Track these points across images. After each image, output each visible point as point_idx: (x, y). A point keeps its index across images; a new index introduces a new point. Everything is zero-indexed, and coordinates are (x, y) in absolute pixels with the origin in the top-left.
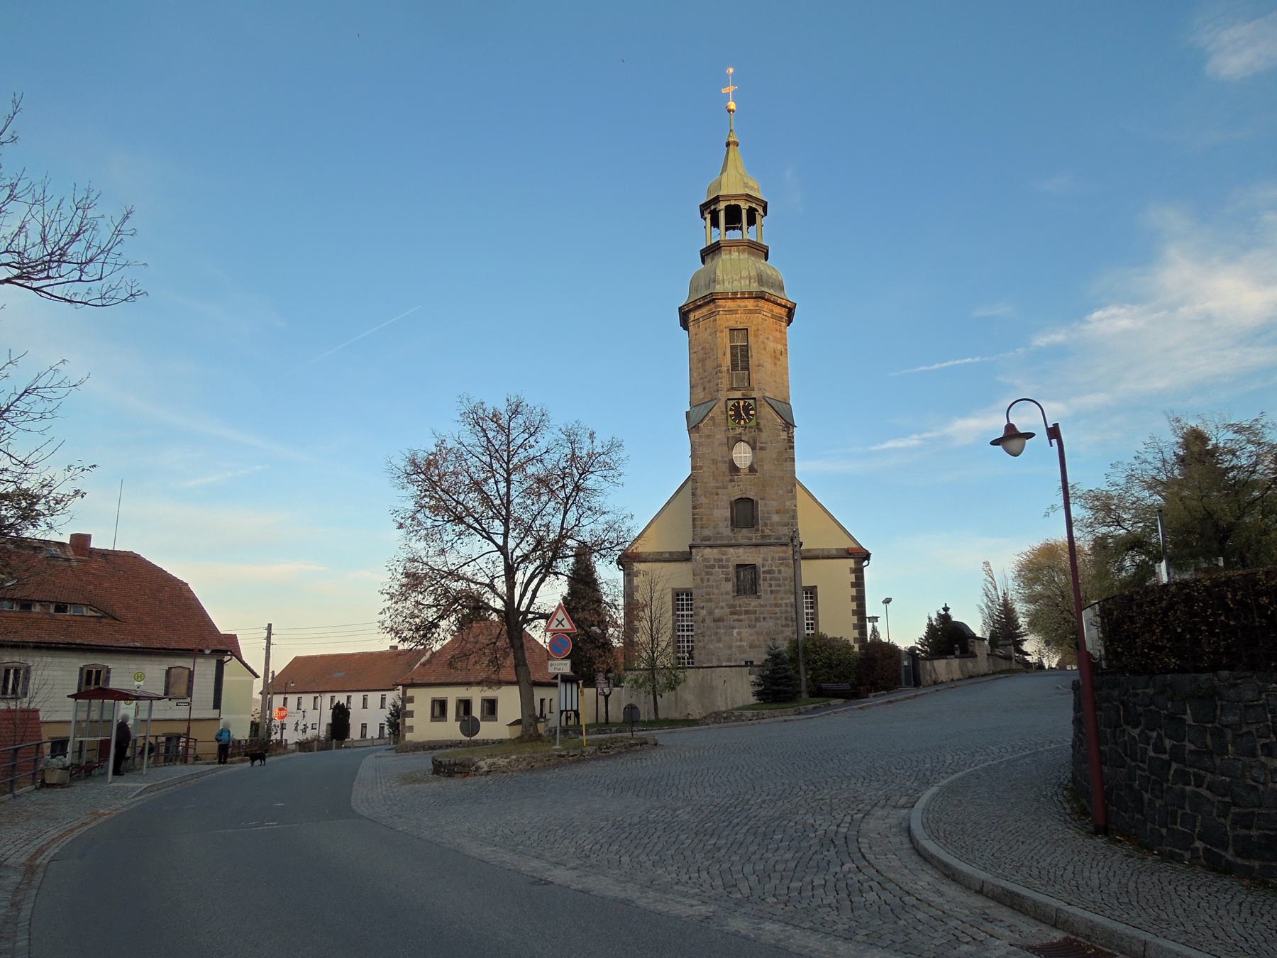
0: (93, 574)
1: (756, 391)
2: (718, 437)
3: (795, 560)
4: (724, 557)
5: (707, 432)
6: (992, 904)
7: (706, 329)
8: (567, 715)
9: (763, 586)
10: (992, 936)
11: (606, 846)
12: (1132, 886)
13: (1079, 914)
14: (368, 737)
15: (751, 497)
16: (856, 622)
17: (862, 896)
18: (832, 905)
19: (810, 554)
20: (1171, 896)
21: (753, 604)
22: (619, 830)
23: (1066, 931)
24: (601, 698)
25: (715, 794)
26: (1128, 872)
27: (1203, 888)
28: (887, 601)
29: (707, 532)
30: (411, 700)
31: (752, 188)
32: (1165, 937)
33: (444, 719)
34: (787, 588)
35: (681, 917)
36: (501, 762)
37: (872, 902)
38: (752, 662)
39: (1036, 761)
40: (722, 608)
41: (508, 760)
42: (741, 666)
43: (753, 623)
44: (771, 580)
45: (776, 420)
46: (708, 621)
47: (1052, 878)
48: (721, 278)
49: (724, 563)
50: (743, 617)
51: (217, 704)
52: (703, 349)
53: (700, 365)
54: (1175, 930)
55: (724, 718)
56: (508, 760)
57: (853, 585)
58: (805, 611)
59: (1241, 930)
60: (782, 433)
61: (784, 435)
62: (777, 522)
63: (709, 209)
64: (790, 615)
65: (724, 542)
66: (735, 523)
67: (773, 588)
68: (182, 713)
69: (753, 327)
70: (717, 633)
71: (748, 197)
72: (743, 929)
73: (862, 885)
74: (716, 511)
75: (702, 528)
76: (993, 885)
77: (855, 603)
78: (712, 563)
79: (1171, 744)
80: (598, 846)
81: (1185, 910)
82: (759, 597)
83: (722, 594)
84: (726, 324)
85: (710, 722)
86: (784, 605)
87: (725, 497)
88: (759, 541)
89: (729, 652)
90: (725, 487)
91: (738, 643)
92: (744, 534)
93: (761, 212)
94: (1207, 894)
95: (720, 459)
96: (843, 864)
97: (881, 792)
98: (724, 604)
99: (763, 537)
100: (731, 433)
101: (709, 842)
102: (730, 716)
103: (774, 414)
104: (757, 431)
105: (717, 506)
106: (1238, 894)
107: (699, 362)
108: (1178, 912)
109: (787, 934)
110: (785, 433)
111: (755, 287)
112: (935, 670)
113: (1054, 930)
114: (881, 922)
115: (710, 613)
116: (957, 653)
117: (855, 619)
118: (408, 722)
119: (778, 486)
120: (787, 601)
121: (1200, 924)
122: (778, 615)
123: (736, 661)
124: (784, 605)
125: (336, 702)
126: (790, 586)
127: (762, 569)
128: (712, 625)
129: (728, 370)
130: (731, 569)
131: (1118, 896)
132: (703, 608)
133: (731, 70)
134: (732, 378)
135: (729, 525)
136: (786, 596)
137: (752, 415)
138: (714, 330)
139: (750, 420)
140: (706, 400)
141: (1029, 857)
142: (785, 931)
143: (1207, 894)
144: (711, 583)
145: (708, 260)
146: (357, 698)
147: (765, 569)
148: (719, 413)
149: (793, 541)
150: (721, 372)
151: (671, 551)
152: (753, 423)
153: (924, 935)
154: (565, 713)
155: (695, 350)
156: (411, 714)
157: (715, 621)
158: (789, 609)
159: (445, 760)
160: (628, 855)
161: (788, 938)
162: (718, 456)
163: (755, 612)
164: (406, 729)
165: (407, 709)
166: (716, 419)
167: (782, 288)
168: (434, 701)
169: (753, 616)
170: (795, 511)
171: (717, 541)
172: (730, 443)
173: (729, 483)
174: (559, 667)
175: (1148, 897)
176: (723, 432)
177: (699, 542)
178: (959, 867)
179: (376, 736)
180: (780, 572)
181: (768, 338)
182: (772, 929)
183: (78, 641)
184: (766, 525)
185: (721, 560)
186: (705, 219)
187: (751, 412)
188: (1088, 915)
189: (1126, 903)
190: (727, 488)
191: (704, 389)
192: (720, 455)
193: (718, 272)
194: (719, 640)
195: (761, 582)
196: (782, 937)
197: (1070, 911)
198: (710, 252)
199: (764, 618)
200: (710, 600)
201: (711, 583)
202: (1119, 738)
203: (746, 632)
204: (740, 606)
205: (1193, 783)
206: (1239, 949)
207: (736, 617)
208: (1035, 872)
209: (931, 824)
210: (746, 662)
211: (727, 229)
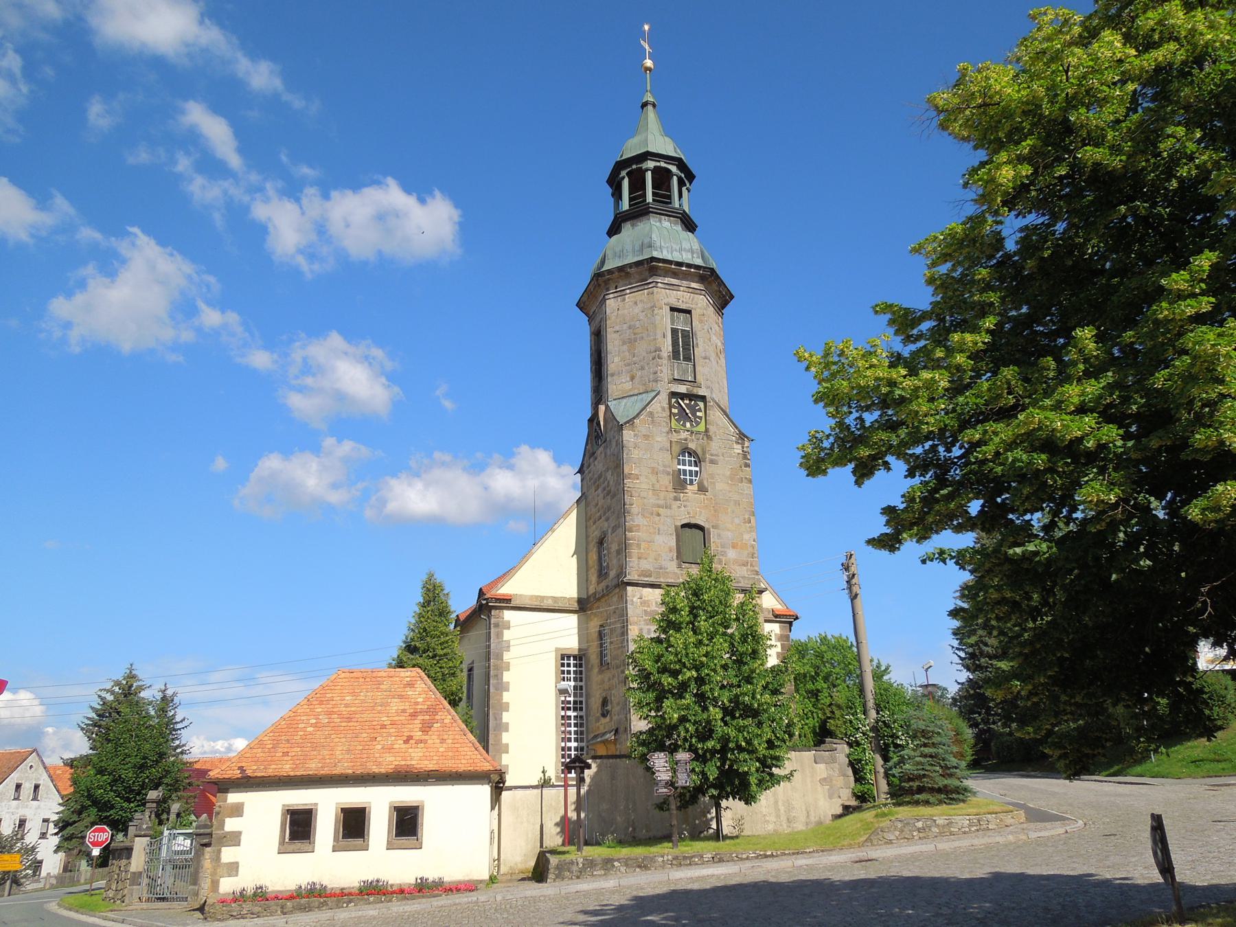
2: (659, 439)
5: (644, 431)
7: (636, 303)
15: (702, 524)
29: (646, 565)
33: (359, 841)
45: (728, 428)
48: (658, 244)
55: (919, 830)
60: (736, 446)
61: (738, 449)
69: (698, 310)
75: (639, 558)
84: (666, 301)
85: (892, 837)
90: (668, 507)
100: (675, 437)
103: (725, 421)
104: (705, 438)
105: (659, 530)
107: (624, 343)
110: (739, 446)
118: (228, 854)
133: (646, 27)
135: (675, 557)
138: (649, 305)
139: (698, 424)
140: (636, 392)
148: (660, 409)
150: (660, 357)
151: (555, 596)
152: (701, 428)
155: (617, 328)
166: (656, 415)
171: (659, 578)
172: (673, 448)
173: (674, 502)
176: (665, 434)
177: (636, 577)
190: (670, 508)
191: (632, 378)
192: (661, 463)
193: (654, 237)
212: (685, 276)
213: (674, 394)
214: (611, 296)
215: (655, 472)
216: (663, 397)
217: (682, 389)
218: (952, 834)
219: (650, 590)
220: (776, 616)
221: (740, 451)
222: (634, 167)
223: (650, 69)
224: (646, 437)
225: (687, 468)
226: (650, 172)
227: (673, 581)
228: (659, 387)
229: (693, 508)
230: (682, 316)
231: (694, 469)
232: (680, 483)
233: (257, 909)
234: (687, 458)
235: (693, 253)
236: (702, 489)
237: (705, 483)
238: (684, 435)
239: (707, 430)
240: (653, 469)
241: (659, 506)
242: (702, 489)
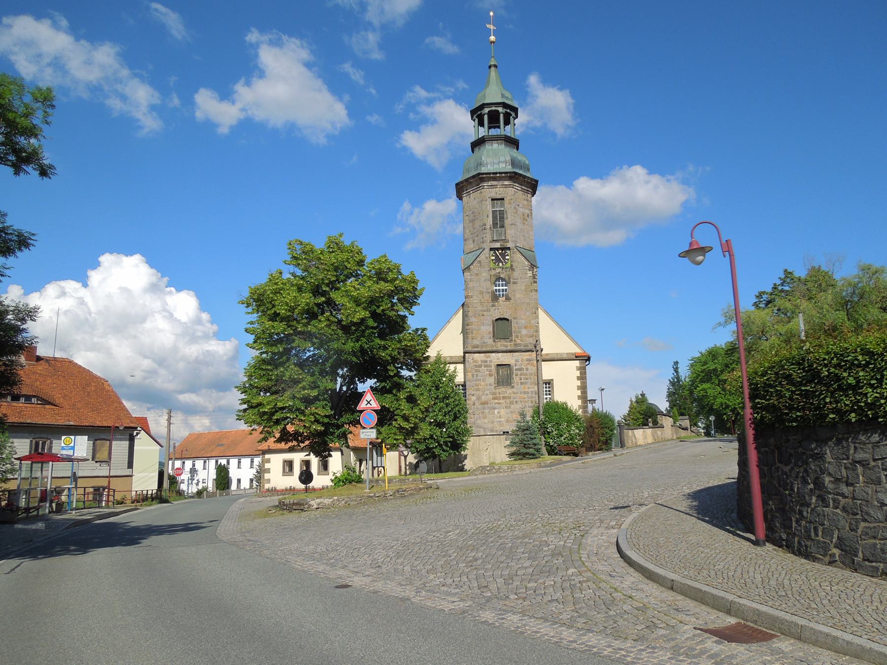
0: (39, 374)
1: (510, 243)
2: (484, 275)
3: (538, 361)
4: (488, 359)
5: (476, 272)
6: (680, 597)
7: (475, 199)
8: (378, 470)
9: (516, 379)
10: (681, 622)
11: (394, 559)
12: (786, 582)
13: (748, 604)
14: (242, 488)
15: (507, 318)
16: (580, 404)
17: (582, 593)
18: (559, 600)
19: (548, 357)
20: (467, 577)
21: (508, 392)
22: (405, 548)
23: (738, 618)
24: (403, 458)
25: (477, 521)
26: (783, 572)
27: (841, 584)
28: (603, 390)
29: (476, 342)
30: (268, 461)
31: (507, 98)
32: (816, 622)
33: (326, 472)
34: (532, 380)
35: (444, 611)
36: (327, 501)
37: (589, 598)
38: (508, 432)
39: (709, 494)
40: (487, 395)
41: (332, 500)
42: (500, 435)
43: (509, 405)
44: (521, 375)
46: (477, 404)
47: (726, 577)
48: (485, 162)
49: (488, 363)
50: (501, 401)
51: (130, 465)
52: (472, 213)
53: (471, 224)
54: (823, 616)
56: (332, 500)
57: (578, 378)
58: (545, 397)
59: (875, 616)
60: (528, 272)
61: (530, 274)
62: (525, 335)
63: (476, 113)
64: (534, 399)
65: (488, 349)
66: (496, 336)
67: (523, 381)
68: (103, 471)
70: (483, 412)
71: (504, 105)
72: (490, 619)
73: (582, 585)
74: (482, 327)
76: (681, 583)
77: (580, 391)
78: (480, 363)
79: (815, 476)
80: (389, 559)
81: (829, 600)
82: (513, 387)
83: (487, 385)
84: (488, 196)
86: (530, 392)
87: (489, 317)
88: (513, 348)
89: (492, 425)
90: (488, 310)
91: (498, 419)
92: (501, 345)
93: (513, 115)
94: (845, 588)
95: (485, 291)
96: (568, 569)
97: (597, 518)
98: (488, 392)
99: (515, 345)
100: (493, 272)
101: (470, 555)
102: (492, 469)
103: (523, 258)
106: (868, 587)
108: (824, 602)
109: (524, 622)
110: (531, 272)
111: (509, 168)
112: (635, 436)
113: (729, 617)
114: (596, 613)
115: (479, 398)
116: (650, 424)
117: (579, 383)
119: (526, 309)
120: (532, 390)
121: (842, 611)
122: (527, 399)
123: (497, 431)
124: (530, 392)
125: (219, 463)
126: (534, 379)
127: (515, 368)
128: (480, 406)
129: (490, 228)
130: (493, 368)
131: (777, 590)
132: (473, 395)
134: (493, 232)
136: (531, 386)
137: (508, 259)
139: (506, 263)
141: (707, 563)
142: (522, 620)
143: (845, 588)
144: (479, 378)
145: (476, 150)
146: (234, 462)
147: (517, 367)
149: (536, 348)
153: (629, 622)
154: (377, 468)
155: (467, 214)
156: (268, 471)
157: (482, 404)
158: (534, 395)
159: (287, 501)
160: (409, 565)
161: (525, 625)
162: (483, 288)
163: (510, 398)
164: (265, 482)
165: (266, 467)
166: (482, 262)
167: (528, 170)
168: (285, 461)
169: (508, 401)
170: (537, 327)
174: (368, 434)
175: (800, 591)
178: (655, 571)
179: (248, 487)
180: (527, 369)
181: (518, 205)
182: (513, 619)
183: (29, 421)
184: (517, 337)
185: (486, 362)
186: (474, 120)
187: (507, 257)
188: (755, 605)
189: (784, 596)
191: (474, 241)
193: (483, 158)
194: (485, 418)
195: (514, 376)
196: (520, 625)
197: (741, 602)
198: (478, 144)
199: (516, 402)
200: (478, 390)
201: (479, 378)
202: (774, 474)
203: (503, 412)
204: (499, 394)
205: (831, 505)
206: (876, 630)
207: (497, 401)
208: (713, 573)
209: (634, 539)
210: (504, 432)
211: (490, 128)
212: (500, 179)
213: (491, 249)
214: (465, 195)
215: (481, 293)
216: (487, 250)
217: (498, 245)
218: (501, 472)
219: (478, 354)
220: (576, 357)
221: (531, 275)
222: (479, 113)
223: (494, 42)
224: (477, 275)
225: (501, 288)
226: (486, 115)
227: (490, 349)
228: (484, 246)
229: (502, 309)
230: (499, 202)
231: (504, 288)
232: (495, 297)
233: (270, 494)
234: (501, 283)
235: (506, 163)
236: (508, 298)
237: (510, 295)
238: (498, 270)
239: (512, 266)
240: (480, 291)
241: (483, 311)
242: (508, 298)
